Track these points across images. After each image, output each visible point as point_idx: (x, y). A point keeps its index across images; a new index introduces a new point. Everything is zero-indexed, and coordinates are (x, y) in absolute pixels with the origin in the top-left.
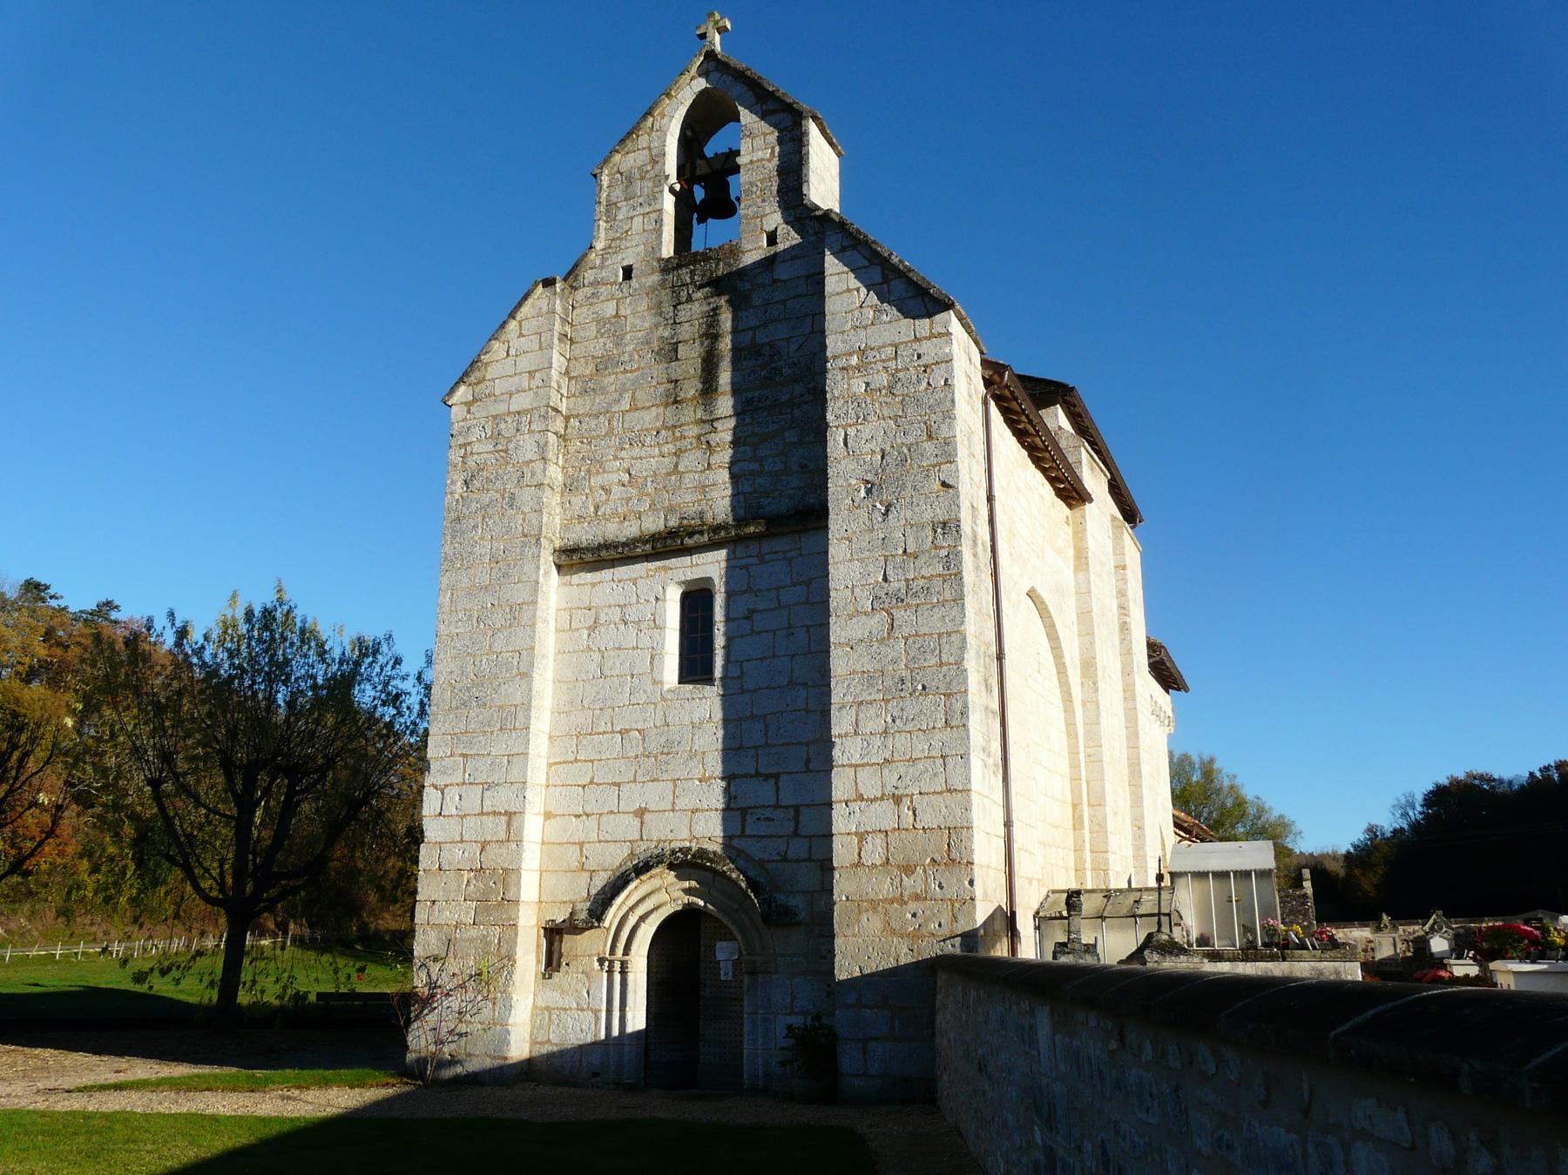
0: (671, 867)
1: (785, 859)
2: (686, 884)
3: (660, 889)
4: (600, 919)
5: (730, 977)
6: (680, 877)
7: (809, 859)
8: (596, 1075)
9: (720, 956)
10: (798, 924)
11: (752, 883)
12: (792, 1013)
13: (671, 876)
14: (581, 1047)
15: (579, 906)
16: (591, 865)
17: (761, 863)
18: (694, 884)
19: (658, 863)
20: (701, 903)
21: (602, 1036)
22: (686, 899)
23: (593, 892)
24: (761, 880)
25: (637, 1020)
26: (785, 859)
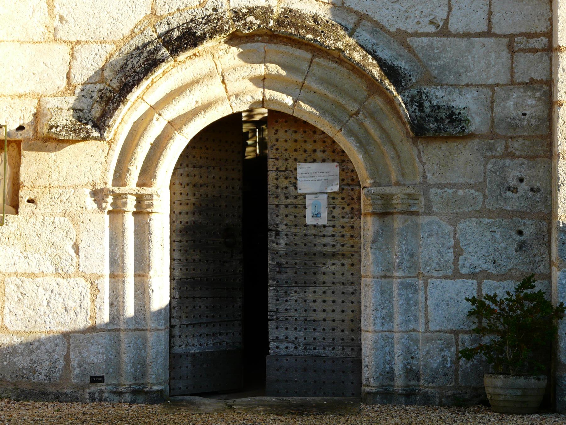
0: (234, 39)
1: (443, 31)
2: (260, 69)
3: (210, 75)
4: (101, 124)
5: (323, 220)
6: (246, 57)
7: (488, 34)
8: (96, 380)
9: (304, 185)
10: (472, 136)
11: (390, 71)
12: (456, 275)
13: (230, 56)
14: (66, 336)
15: (51, 103)
16: (70, 32)
17: (401, 37)
18: (274, 69)
19: (214, 32)
20: (289, 101)
21: (105, 317)
22: (258, 94)
23: (79, 78)
24: (402, 64)
25: (160, 296)
26: (443, 31)
